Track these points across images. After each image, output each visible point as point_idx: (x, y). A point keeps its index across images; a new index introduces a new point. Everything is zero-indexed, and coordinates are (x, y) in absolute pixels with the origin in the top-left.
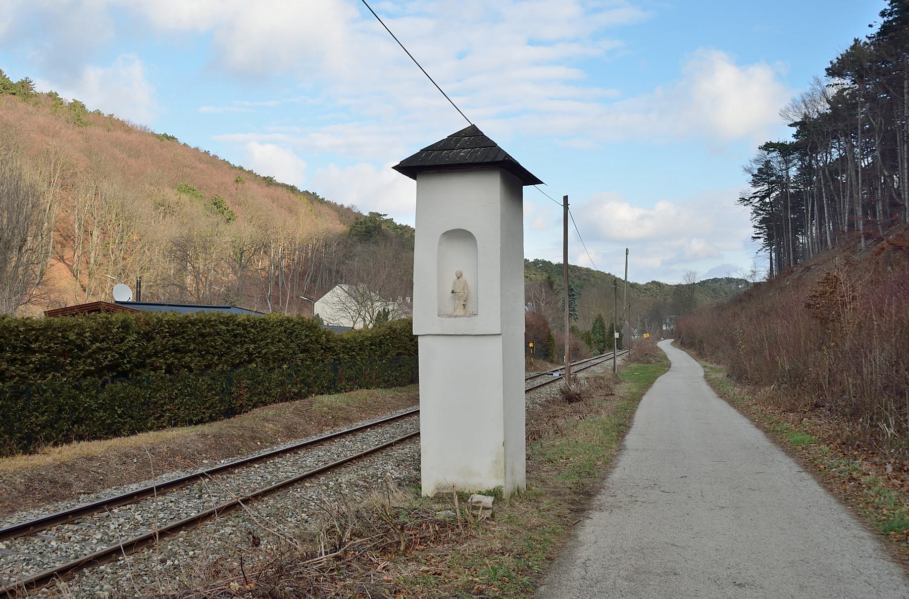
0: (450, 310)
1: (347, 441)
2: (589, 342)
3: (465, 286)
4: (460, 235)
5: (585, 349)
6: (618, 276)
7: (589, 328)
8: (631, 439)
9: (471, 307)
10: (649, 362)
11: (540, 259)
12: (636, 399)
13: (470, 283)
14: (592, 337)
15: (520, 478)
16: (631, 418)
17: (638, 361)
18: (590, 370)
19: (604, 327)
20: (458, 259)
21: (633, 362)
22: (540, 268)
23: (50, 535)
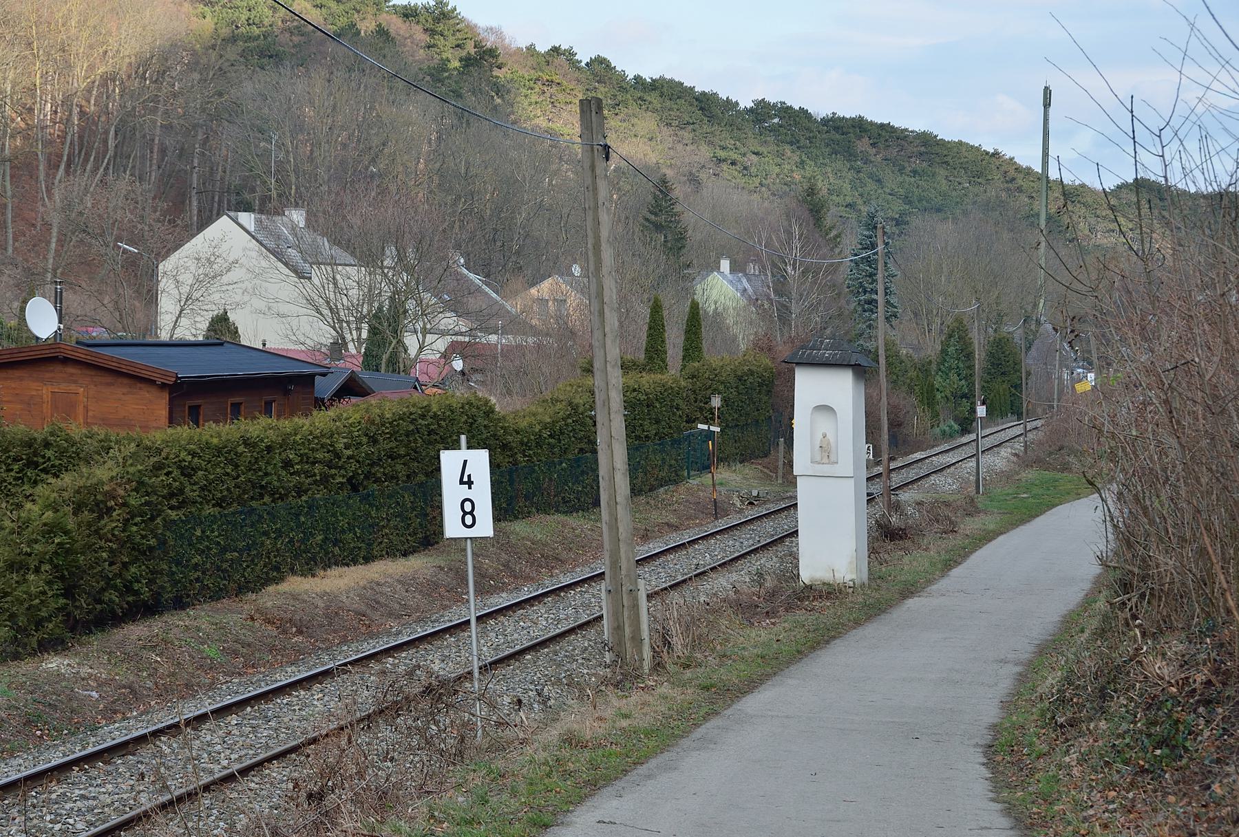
0: (818, 459)
1: (507, 622)
2: (928, 398)
3: (829, 444)
4: (825, 409)
5: (917, 421)
6: (1023, 162)
7: (932, 349)
8: (956, 572)
9: (833, 458)
10: (1066, 468)
11: (772, 99)
12: (988, 537)
13: (832, 441)
14: (938, 381)
15: (865, 576)
16: (966, 556)
17: (1039, 462)
18: (926, 483)
19: (969, 356)
20: (824, 425)
21: (1029, 465)
22: (773, 130)
23: (209, 734)
